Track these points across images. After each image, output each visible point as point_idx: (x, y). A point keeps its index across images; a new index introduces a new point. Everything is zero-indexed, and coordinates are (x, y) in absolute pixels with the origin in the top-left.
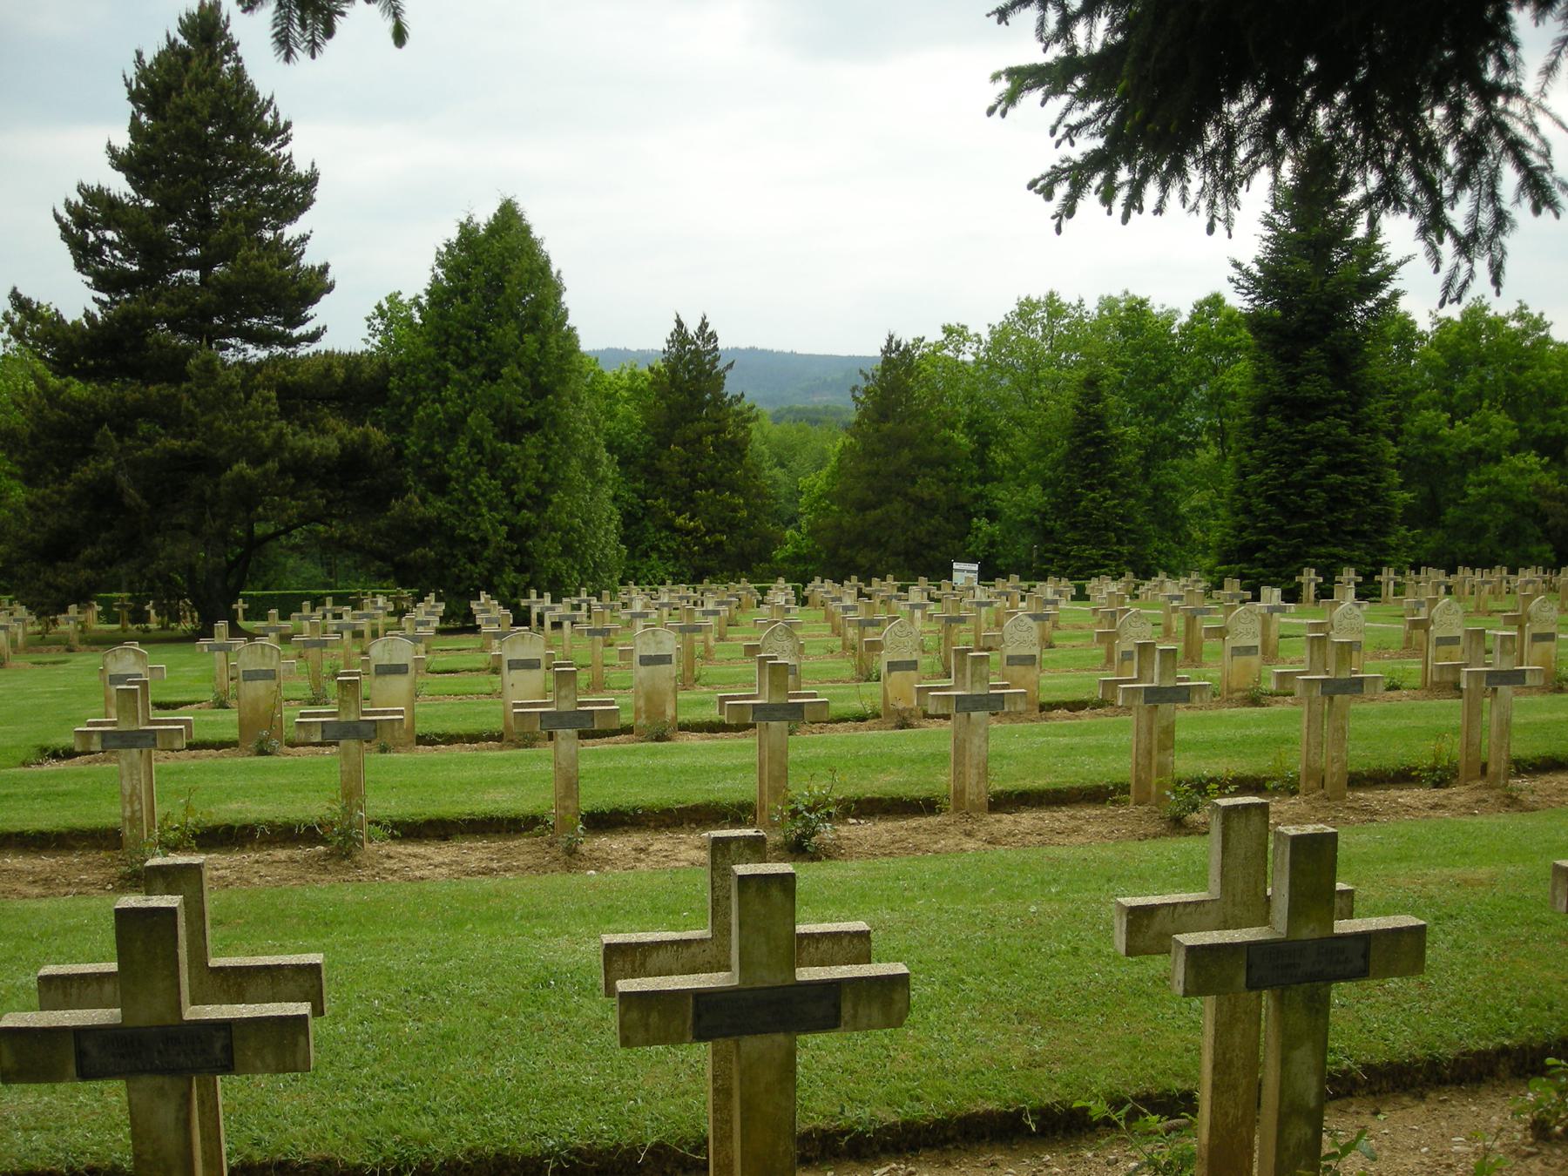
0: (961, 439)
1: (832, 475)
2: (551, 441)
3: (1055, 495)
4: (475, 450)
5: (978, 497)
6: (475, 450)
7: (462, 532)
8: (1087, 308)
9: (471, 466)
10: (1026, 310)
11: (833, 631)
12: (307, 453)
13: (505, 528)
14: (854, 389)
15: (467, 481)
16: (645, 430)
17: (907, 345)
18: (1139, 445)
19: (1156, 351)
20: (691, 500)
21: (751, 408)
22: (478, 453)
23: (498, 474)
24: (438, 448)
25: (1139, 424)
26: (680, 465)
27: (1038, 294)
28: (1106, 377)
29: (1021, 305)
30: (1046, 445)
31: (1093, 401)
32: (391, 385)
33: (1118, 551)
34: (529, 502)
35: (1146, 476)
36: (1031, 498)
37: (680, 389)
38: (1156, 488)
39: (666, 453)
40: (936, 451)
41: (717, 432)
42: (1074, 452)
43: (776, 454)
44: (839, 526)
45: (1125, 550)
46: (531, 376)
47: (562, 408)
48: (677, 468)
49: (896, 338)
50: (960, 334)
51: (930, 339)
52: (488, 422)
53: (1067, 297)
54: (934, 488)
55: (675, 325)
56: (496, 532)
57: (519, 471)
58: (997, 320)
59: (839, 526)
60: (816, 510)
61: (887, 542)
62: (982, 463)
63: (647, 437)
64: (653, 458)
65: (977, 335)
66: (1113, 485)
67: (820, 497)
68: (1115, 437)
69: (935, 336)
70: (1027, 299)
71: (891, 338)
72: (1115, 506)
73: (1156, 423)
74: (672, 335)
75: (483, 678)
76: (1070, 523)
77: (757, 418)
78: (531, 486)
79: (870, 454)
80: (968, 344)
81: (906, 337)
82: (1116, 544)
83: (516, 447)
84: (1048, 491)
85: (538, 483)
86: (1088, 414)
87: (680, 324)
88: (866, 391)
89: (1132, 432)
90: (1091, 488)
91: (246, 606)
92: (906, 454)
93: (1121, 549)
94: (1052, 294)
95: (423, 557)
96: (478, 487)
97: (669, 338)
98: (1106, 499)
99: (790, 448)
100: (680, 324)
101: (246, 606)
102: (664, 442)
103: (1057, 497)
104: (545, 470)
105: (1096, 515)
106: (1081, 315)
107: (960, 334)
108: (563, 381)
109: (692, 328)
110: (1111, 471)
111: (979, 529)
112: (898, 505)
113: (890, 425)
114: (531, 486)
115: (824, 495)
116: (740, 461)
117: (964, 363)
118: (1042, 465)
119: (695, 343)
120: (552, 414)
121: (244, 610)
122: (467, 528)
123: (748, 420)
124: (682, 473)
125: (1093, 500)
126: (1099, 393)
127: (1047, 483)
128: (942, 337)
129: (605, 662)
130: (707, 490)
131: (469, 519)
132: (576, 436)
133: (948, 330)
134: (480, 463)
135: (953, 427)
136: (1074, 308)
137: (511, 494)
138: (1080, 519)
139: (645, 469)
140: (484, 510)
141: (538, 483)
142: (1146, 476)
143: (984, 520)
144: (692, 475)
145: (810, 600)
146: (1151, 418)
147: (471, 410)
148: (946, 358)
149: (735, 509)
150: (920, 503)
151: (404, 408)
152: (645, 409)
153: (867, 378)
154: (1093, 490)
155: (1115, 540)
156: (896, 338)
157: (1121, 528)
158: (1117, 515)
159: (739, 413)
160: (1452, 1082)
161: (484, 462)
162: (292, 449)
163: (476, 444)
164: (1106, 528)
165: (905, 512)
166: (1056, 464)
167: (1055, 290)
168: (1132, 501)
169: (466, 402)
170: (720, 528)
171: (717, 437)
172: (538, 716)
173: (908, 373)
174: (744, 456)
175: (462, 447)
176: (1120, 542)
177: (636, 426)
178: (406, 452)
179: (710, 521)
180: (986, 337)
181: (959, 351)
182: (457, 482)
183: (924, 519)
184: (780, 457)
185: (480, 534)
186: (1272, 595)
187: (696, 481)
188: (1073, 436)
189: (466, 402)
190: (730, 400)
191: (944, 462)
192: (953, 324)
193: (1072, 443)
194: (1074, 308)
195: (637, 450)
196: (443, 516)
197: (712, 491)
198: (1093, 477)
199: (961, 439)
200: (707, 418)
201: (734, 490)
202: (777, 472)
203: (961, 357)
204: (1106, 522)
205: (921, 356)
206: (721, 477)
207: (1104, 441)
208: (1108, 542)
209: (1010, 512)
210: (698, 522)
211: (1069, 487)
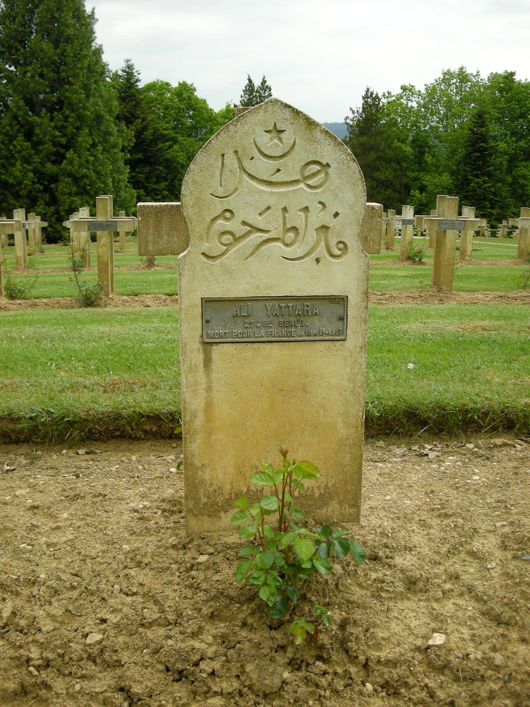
0: (408, 149)
3: (457, 180)
5: (416, 179)
8: (482, 77)
10: (447, 77)
14: (347, 118)
17: (377, 94)
18: (506, 153)
19: (519, 101)
25: (507, 142)
27: (455, 68)
28: (489, 113)
29: (444, 74)
30: (454, 152)
31: (480, 127)
33: (490, 212)
35: (510, 171)
36: (443, 180)
38: (514, 179)
40: (390, 153)
42: (468, 156)
45: (494, 212)
49: (371, 90)
50: (410, 90)
53: (470, 70)
55: (247, 82)
66: (489, 175)
68: (492, 147)
70: (448, 70)
71: (368, 90)
72: (490, 187)
73: (517, 142)
74: (246, 87)
76: (464, 196)
81: (379, 90)
82: (489, 208)
84: (453, 177)
86: (477, 134)
87: (250, 80)
89: (502, 145)
90: (477, 176)
93: (492, 211)
94: (462, 68)
97: (244, 89)
98: (485, 183)
100: (250, 80)
103: (458, 181)
105: (479, 191)
106: (477, 81)
107: (410, 90)
109: (257, 83)
110: (488, 167)
111: (414, 196)
118: (451, 163)
125: (477, 183)
126: (484, 122)
127: (453, 173)
133: (404, 88)
135: (403, 142)
136: (474, 76)
138: (470, 193)
142: (510, 171)
146: (514, 139)
153: (353, 112)
154: (478, 178)
155: (489, 206)
156: (371, 90)
157: (493, 200)
158: (491, 191)
160: (24, 442)
164: (485, 199)
166: (459, 163)
167: (464, 66)
168: (500, 184)
173: (377, 111)
176: (492, 207)
180: (423, 91)
186: (391, 211)
188: (469, 146)
192: (407, 84)
193: (467, 150)
194: (474, 76)
198: (478, 170)
199: (408, 149)
203: (410, 104)
204: (484, 196)
207: (485, 149)
208: (485, 207)
211: (465, 175)
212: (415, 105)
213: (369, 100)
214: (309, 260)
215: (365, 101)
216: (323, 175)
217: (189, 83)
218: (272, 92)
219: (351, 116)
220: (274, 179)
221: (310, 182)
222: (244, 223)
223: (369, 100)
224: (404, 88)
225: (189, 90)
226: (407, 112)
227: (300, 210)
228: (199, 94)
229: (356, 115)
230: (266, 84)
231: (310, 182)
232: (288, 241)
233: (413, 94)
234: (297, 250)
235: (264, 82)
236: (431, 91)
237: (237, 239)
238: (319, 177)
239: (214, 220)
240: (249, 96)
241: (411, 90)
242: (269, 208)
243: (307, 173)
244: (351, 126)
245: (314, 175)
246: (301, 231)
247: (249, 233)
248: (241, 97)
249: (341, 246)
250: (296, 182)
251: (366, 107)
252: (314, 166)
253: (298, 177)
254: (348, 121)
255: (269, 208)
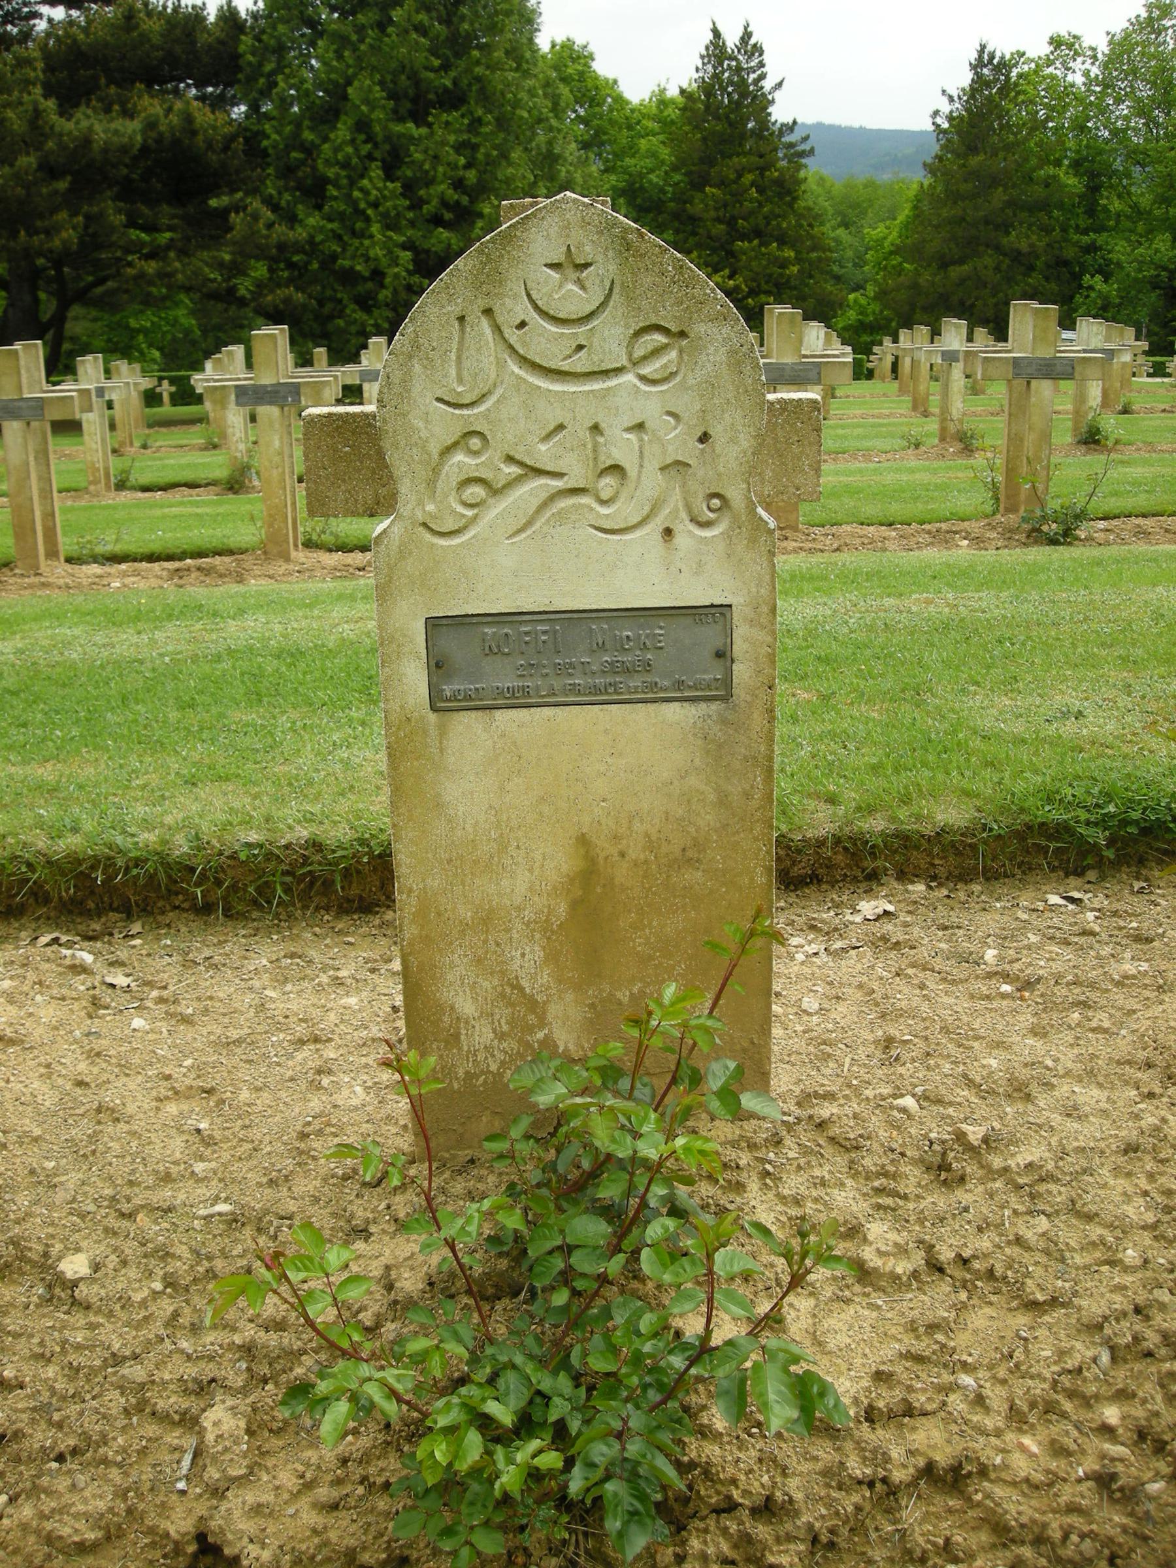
1: (906, 226)
2: (477, 122)
4: (362, 137)
5: (1092, 248)
6: (362, 137)
7: (347, 263)
9: (355, 160)
11: (915, 408)
12: (86, 141)
13: (407, 255)
14: (936, 113)
15: (352, 183)
16: (675, 168)
17: (1002, 58)
20: (731, 254)
21: (805, 139)
22: (366, 142)
23: (399, 173)
24: (308, 136)
26: (716, 209)
32: (242, 48)
34: (448, 216)
36: (1157, 251)
37: (717, 118)
39: (699, 195)
41: (762, 169)
43: (840, 213)
44: (915, 286)
46: (447, 21)
47: (493, 67)
48: (713, 214)
49: (989, 48)
50: (1070, 46)
51: (1032, 54)
52: (378, 93)
54: (1034, 237)
55: (710, 36)
56: (395, 262)
57: (427, 167)
58: (1119, 25)
59: (915, 286)
60: (885, 268)
61: (973, 306)
62: (1091, 212)
63: (677, 177)
64: (685, 202)
65: (1094, 49)
67: (891, 253)
69: (1039, 49)
71: (983, 47)
74: (707, 48)
75: (206, 502)
77: (812, 152)
78: (443, 188)
79: (954, 197)
80: (1079, 60)
81: (1003, 47)
83: (423, 131)
85: (458, 184)
87: (716, 33)
88: (950, 118)
91: (173, 389)
92: (999, 196)
95: (287, 300)
96: (366, 192)
99: (855, 206)
100: (716, 33)
101: (173, 389)
102: (698, 183)
104: (468, 166)
107: (1070, 46)
108: (493, 28)
109: (732, 39)
111: (1091, 288)
112: (988, 260)
113: (981, 157)
114: (443, 188)
115: (896, 251)
116: (791, 205)
117: (1072, 85)
119: (735, 59)
120: (478, 79)
121: (172, 395)
122: (353, 257)
123: (802, 154)
124: (718, 220)
128: (1045, 49)
129: (1056, 408)
130: (750, 241)
131: (356, 242)
132: (519, 112)
133: (1056, 42)
134: (370, 157)
135: (1058, 163)
137: (417, 204)
139: (676, 216)
140: (375, 229)
141: (458, 184)
143: (1098, 278)
144: (731, 222)
145: (876, 373)
147: (355, 75)
148: (1053, 77)
149: (783, 265)
150: (1017, 257)
151: (262, 81)
152: (672, 140)
156: (989, 48)
159: (791, 145)
161: (377, 154)
162: (61, 135)
163: (363, 126)
165: (997, 269)
169: (348, 66)
170: (765, 287)
171: (762, 175)
172: (578, 189)
174: (795, 199)
175: (342, 131)
177: (663, 162)
178: (265, 143)
179: (753, 280)
180: (1103, 48)
181: (1068, 69)
182: (337, 187)
183: (1020, 277)
184: (844, 216)
185: (372, 265)
187: (737, 231)
189: (348, 66)
190: (780, 130)
191: (1044, 206)
192: (1064, 33)
195: (665, 193)
196: (319, 238)
197: (756, 242)
200: (750, 152)
201: (782, 241)
202: (841, 232)
203: (1070, 78)
205: (1020, 76)
206: (768, 224)
209: (1130, 269)
210: (739, 280)
212: (1078, 79)
213: (985, 71)
214: (653, 529)
215: (976, 73)
216: (673, 354)
217: (579, 41)
218: (766, 58)
219: (945, 107)
220: (565, 366)
221: (646, 370)
222: (510, 459)
223: (985, 71)
224: (1056, 42)
225: (579, 57)
226: (1063, 94)
227: (629, 430)
228: (602, 67)
229: (957, 105)
230: (752, 41)
231: (646, 370)
232: (605, 496)
233: (1077, 53)
234: (625, 511)
235: (747, 35)
236: (1121, 47)
237: (495, 491)
238: (664, 360)
239: (448, 450)
240: (715, 68)
241: (1073, 44)
242: (561, 427)
243: (639, 352)
244: (945, 132)
245: (657, 352)
246: (632, 472)
247: (518, 479)
248: (697, 70)
249: (716, 502)
250: (619, 371)
251: (979, 83)
252: (647, 337)
253: (624, 361)
254: (939, 120)
255: (561, 427)
